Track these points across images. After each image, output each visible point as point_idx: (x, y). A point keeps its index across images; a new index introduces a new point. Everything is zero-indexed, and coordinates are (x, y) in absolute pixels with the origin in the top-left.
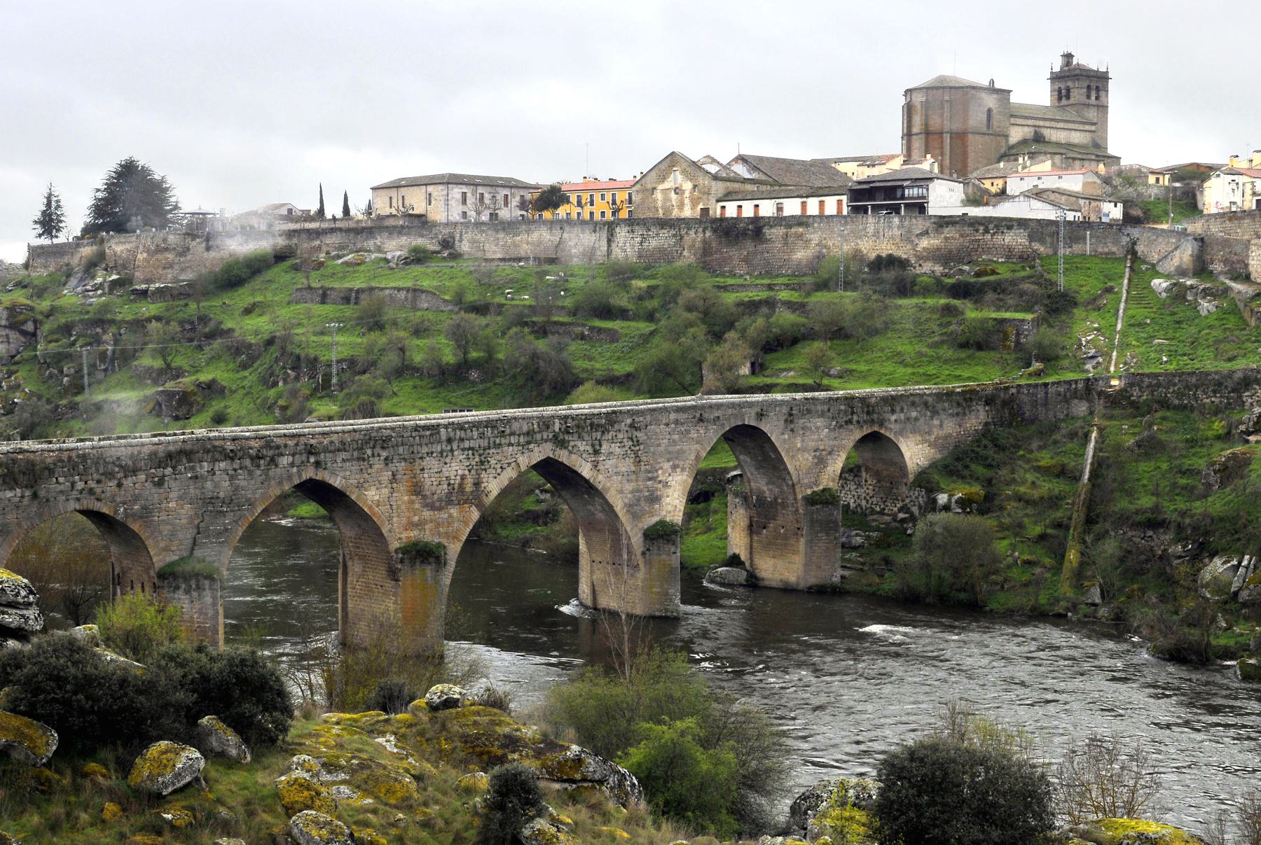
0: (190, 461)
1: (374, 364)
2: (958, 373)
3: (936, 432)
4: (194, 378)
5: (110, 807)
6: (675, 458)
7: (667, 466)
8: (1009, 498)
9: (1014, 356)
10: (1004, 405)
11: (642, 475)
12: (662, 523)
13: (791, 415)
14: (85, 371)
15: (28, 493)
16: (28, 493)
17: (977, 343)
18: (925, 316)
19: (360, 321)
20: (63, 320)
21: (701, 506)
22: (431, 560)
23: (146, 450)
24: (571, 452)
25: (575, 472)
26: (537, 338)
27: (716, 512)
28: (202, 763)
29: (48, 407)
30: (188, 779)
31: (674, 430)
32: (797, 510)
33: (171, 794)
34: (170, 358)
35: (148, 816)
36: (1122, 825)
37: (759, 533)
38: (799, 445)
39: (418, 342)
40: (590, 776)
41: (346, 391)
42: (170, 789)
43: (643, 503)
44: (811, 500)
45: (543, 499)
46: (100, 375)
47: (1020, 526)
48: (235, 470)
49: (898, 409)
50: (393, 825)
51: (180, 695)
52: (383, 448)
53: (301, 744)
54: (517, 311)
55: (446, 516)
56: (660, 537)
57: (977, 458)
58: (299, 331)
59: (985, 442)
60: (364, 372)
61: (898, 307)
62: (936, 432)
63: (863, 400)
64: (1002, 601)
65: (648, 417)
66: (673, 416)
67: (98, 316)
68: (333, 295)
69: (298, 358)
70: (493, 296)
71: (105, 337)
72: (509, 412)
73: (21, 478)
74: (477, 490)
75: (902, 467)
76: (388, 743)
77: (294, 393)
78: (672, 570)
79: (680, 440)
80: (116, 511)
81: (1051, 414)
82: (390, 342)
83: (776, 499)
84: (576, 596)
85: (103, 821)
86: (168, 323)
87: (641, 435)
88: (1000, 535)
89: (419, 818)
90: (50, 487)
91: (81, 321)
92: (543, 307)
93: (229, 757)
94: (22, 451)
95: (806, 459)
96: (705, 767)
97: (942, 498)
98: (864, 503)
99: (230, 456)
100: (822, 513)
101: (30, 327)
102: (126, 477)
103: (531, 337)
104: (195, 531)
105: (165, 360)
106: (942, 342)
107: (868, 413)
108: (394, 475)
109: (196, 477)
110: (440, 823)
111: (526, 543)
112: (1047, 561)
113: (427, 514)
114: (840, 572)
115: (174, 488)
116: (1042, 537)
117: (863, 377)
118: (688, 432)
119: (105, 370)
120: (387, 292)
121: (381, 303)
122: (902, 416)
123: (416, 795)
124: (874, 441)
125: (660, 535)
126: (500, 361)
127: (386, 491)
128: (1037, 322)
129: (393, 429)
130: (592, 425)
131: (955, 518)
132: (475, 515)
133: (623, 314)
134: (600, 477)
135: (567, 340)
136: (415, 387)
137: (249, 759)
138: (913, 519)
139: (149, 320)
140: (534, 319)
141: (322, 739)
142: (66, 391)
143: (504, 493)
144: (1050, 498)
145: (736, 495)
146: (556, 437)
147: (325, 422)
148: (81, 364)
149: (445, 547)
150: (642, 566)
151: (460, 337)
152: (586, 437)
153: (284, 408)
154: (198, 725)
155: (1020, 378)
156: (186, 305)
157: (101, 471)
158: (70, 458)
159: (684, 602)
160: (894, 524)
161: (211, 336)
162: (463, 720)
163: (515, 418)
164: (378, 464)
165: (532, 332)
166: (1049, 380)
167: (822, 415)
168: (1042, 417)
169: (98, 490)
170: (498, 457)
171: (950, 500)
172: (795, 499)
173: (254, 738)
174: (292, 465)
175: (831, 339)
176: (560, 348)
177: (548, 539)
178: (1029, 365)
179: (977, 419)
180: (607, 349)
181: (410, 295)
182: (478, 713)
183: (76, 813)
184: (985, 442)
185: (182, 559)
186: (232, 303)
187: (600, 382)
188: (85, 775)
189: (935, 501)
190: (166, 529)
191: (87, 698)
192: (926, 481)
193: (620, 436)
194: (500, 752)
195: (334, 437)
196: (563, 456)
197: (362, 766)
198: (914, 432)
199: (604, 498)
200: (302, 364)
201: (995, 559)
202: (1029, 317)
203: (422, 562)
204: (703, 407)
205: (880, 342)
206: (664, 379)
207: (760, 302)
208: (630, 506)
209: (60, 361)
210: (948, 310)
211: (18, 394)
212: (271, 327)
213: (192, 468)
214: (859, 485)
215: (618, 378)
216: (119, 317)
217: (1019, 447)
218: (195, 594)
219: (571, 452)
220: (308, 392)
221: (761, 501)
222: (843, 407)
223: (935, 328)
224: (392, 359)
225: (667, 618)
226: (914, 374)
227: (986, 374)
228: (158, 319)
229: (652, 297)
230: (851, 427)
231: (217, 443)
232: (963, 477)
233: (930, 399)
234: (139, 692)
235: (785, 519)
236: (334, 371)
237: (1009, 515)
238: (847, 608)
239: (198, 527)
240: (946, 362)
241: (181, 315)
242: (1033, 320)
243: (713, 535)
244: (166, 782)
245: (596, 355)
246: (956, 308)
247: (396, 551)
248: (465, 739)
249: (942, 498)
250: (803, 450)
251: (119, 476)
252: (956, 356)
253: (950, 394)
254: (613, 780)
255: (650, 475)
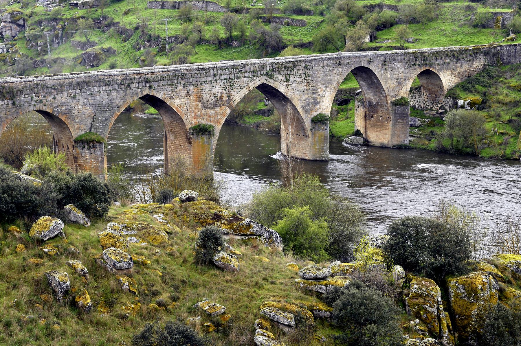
0: (88, 86)
1: (186, 38)
2: (472, 40)
3: (459, 69)
4: (100, 46)
5: (20, 246)
6: (327, 83)
7: (323, 87)
8: (494, 102)
9: (501, 31)
10: (494, 55)
11: (310, 92)
12: (320, 115)
13: (385, 61)
14: (48, 44)
15: (10, 102)
16: (10, 102)
17: (482, 25)
18: (457, 11)
19: (180, 17)
20: (37, 19)
21: (344, 107)
22: (207, 133)
23: (67, 81)
24: (275, 81)
25: (277, 90)
26: (266, 25)
27: (350, 110)
28: (63, 226)
29: (32, 61)
30: (56, 233)
31: (326, 69)
32: (388, 108)
33: (48, 240)
34: (89, 37)
35: (37, 250)
36: (509, 257)
37: (369, 120)
38: (389, 76)
39: (208, 27)
40: (254, 233)
41: (173, 52)
42: (48, 238)
43: (311, 105)
44: (395, 104)
45: (264, 104)
46: (56, 46)
47: (499, 115)
48: (110, 90)
49: (439, 58)
50: (154, 255)
51: (54, 195)
52: (182, 79)
53: (116, 218)
54: (256, 11)
55: (214, 112)
56: (319, 121)
57: (479, 82)
58: (151, 22)
59: (483, 74)
60: (182, 43)
61: (444, 7)
62: (459, 69)
63: (421, 54)
64: (488, 152)
65: (313, 63)
66: (326, 62)
67: (54, 17)
68: (167, 5)
69: (150, 36)
70: (245, 4)
71: (57, 27)
72: (244, 61)
73: (7, 95)
74: (229, 99)
75: (442, 87)
76: (159, 217)
77: (148, 53)
78: (325, 138)
79: (329, 74)
80: (53, 111)
81: (518, 60)
82: (194, 27)
83: (377, 103)
84: (280, 150)
85: (16, 252)
86: (87, 19)
87: (309, 72)
88: (489, 120)
89: (167, 252)
90: (21, 99)
91: (46, 19)
92: (269, 9)
93: (79, 224)
94: (7, 82)
95: (392, 83)
96: (312, 229)
97: (460, 102)
98: (422, 105)
99: (108, 84)
100: (400, 110)
101: (21, 22)
102: (57, 94)
103: (263, 24)
104: (92, 120)
105: (86, 38)
106: (465, 25)
107: (424, 60)
108: (188, 92)
109: (92, 94)
110: (178, 254)
111: (258, 125)
112: (512, 133)
113: (204, 111)
114: (410, 138)
115: (81, 99)
116: (510, 121)
117: (425, 42)
118: (333, 70)
119: (58, 43)
120: (193, 3)
121: (190, 8)
122: (442, 62)
123: (167, 241)
124: (427, 74)
125: (319, 121)
126: (247, 36)
127: (184, 100)
128: (514, 14)
129: (187, 70)
130: (285, 67)
131: (467, 113)
132: (228, 111)
133: (308, 12)
134: (290, 93)
135: (280, 25)
136: (206, 50)
137: (89, 224)
138: (446, 112)
139: (79, 18)
140: (265, 15)
141: (127, 216)
142: (39, 54)
143: (242, 101)
144: (515, 102)
145: (359, 101)
146: (267, 73)
147: (163, 65)
148: (46, 40)
149: (213, 127)
150: (310, 136)
151: (228, 25)
152: (282, 73)
153: (144, 61)
154: (63, 209)
155: (503, 42)
156: (96, 10)
157: (45, 91)
158: (30, 85)
159: (331, 152)
160: (437, 115)
161: (109, 26)
162: (196, 207)
163: (247, 64)
164: (180, 87)
165: (264, 22)
166: (517, 43)
167: (401, 61)
168: (513, 61)
169: (44, 101)
170: (239, 83)
171: (464, 103)
172: (387, 103)
173: (91, 215)
174: (138, 88)
175: (409, 24)
176: (277, 29)
177: (268, 123)
178: (508, 35)
179: (479, 63)
180: (300, 30)
181: (204, 4)
182: (203, 204)
183: (4, 249)
184: (483, 74)
185: (86, 133)
186: (118, 9)
187: (295, 46)
188: (9, 231)
189: (457, 103)
190: (78, 119)
191: (9, 196)
192: (452, 94)
193: (299, 72)
194: (211, 222)
195: (158, 74)
196: (271, 83)
197: (143, 228)
198: (447, 69)
199: (291, 103)
200: (152, 39)
201: (486, 132)
202: (509, 11)
203: (202, 134)
204: (340, 58)
205: (434, 24)
206: (326, 44)
207: (375, 5)
208: (305, 106)
209: (36, 39)
210: (469, 8)
211: (17, 55)
212: (137, 21)
213: (90, 90)
214: (420, 96)
215: (305, 44)
216: (64, 17)
217: (500, 77)
218: (92, 150)
219: (275, 81)
220: (155, 53)
221: (370, 104)
222: (411, 57)
223: (462, 17)
224: (195, 36)
225: (322, 161)
226: (450, 40)
227: (487, 40)
228: (83, 17)
229: (322, 4)
230: (416, 67)
231: (100, 77)
232: (471, 92)
233: (456, 53)
234: (33, 193)
235: (382, 112)
236: (167, 42)
237: (494, 110)
238: (410, 156)
239: (93, 118)
240: (466, 34)
241: (94, 16)
242: (511, 12)
243: (349, 120)
244: (46, 234)
245: (294, 33)
246: (473, 7)
247: (190, 129)
248: (196, 215)
249: (460, 102)
250: (391, 78)
251: (54, 94)
252: (471, 31)
253: (466, 50)
254: (266, 235)
255: (313, 90)
